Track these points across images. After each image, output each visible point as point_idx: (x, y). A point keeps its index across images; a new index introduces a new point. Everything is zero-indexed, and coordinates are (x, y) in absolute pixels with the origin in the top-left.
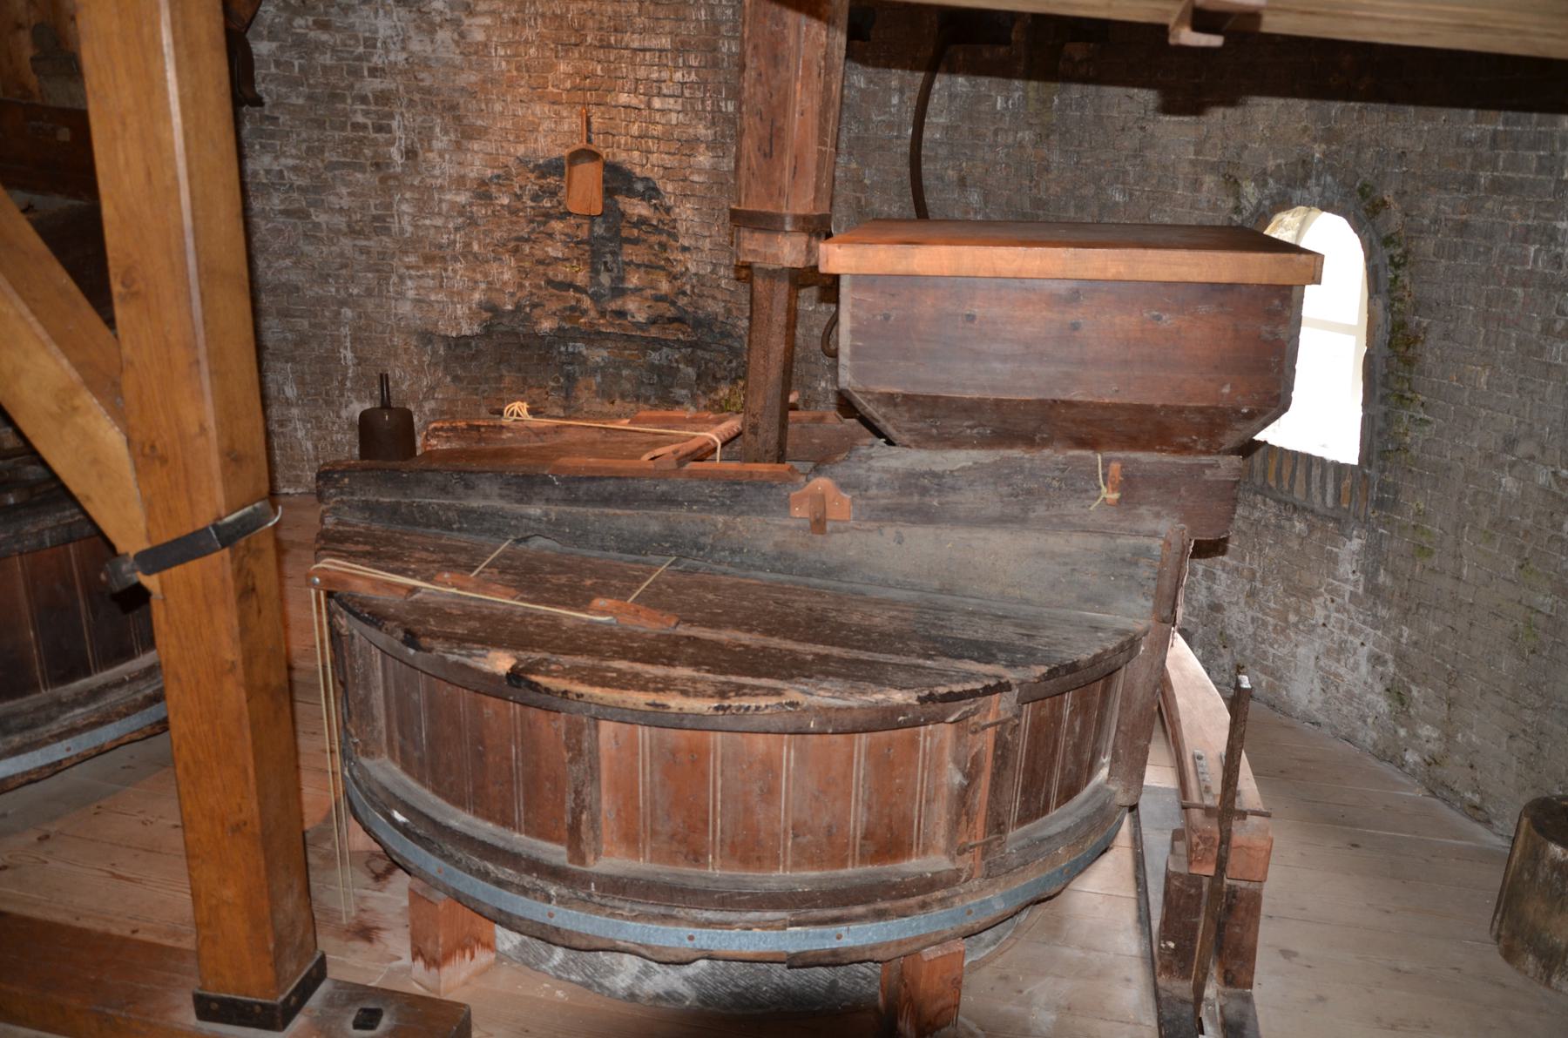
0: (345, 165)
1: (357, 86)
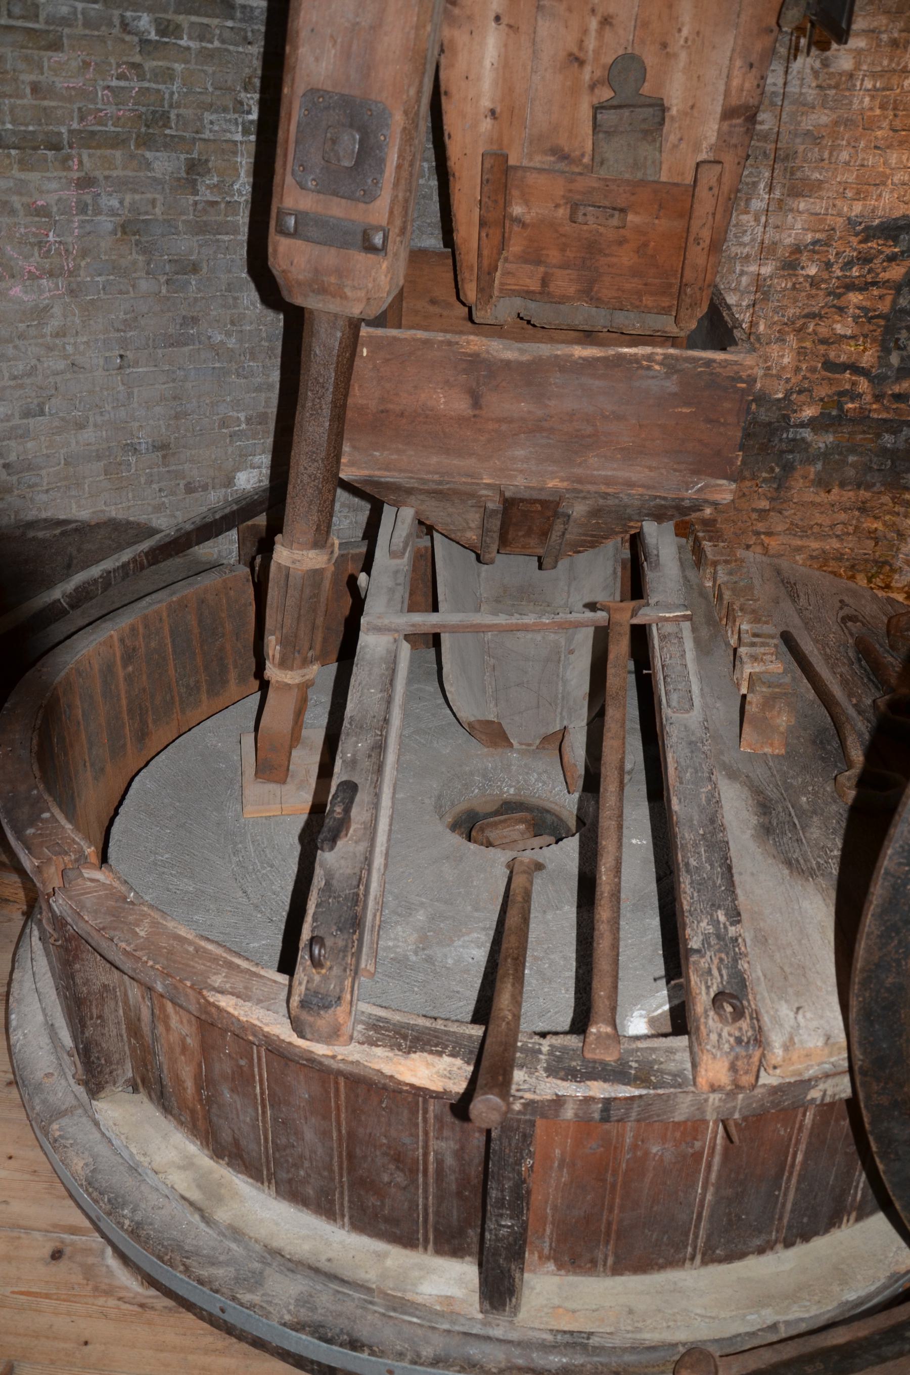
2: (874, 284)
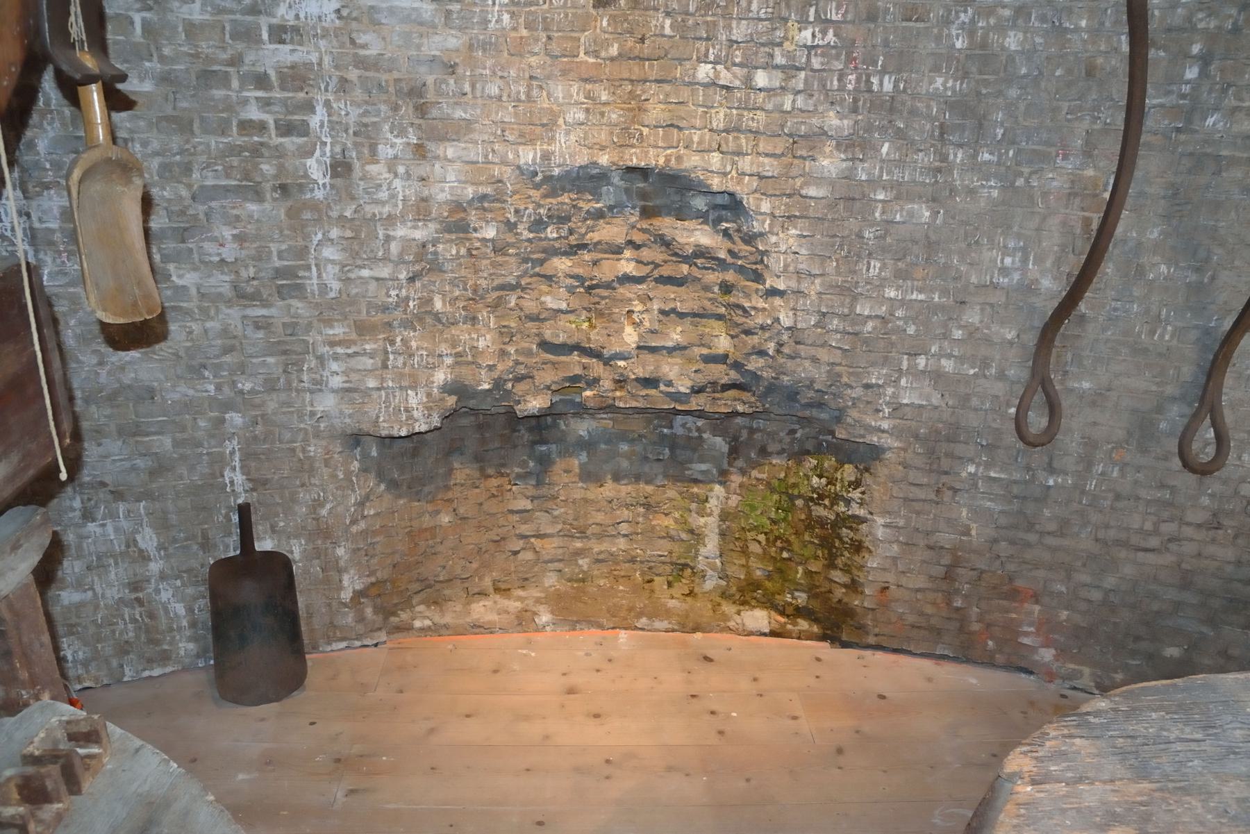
0: (227, 189)
1: (249, 58)
2: (583, 246)
